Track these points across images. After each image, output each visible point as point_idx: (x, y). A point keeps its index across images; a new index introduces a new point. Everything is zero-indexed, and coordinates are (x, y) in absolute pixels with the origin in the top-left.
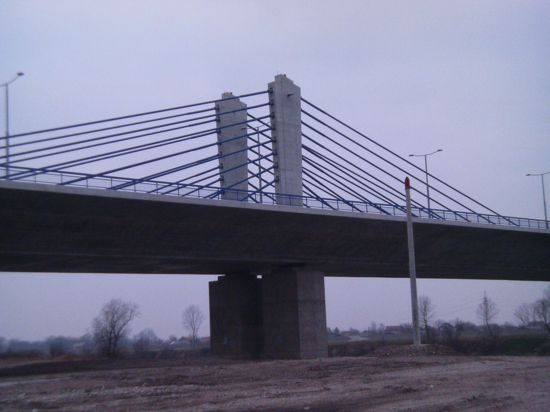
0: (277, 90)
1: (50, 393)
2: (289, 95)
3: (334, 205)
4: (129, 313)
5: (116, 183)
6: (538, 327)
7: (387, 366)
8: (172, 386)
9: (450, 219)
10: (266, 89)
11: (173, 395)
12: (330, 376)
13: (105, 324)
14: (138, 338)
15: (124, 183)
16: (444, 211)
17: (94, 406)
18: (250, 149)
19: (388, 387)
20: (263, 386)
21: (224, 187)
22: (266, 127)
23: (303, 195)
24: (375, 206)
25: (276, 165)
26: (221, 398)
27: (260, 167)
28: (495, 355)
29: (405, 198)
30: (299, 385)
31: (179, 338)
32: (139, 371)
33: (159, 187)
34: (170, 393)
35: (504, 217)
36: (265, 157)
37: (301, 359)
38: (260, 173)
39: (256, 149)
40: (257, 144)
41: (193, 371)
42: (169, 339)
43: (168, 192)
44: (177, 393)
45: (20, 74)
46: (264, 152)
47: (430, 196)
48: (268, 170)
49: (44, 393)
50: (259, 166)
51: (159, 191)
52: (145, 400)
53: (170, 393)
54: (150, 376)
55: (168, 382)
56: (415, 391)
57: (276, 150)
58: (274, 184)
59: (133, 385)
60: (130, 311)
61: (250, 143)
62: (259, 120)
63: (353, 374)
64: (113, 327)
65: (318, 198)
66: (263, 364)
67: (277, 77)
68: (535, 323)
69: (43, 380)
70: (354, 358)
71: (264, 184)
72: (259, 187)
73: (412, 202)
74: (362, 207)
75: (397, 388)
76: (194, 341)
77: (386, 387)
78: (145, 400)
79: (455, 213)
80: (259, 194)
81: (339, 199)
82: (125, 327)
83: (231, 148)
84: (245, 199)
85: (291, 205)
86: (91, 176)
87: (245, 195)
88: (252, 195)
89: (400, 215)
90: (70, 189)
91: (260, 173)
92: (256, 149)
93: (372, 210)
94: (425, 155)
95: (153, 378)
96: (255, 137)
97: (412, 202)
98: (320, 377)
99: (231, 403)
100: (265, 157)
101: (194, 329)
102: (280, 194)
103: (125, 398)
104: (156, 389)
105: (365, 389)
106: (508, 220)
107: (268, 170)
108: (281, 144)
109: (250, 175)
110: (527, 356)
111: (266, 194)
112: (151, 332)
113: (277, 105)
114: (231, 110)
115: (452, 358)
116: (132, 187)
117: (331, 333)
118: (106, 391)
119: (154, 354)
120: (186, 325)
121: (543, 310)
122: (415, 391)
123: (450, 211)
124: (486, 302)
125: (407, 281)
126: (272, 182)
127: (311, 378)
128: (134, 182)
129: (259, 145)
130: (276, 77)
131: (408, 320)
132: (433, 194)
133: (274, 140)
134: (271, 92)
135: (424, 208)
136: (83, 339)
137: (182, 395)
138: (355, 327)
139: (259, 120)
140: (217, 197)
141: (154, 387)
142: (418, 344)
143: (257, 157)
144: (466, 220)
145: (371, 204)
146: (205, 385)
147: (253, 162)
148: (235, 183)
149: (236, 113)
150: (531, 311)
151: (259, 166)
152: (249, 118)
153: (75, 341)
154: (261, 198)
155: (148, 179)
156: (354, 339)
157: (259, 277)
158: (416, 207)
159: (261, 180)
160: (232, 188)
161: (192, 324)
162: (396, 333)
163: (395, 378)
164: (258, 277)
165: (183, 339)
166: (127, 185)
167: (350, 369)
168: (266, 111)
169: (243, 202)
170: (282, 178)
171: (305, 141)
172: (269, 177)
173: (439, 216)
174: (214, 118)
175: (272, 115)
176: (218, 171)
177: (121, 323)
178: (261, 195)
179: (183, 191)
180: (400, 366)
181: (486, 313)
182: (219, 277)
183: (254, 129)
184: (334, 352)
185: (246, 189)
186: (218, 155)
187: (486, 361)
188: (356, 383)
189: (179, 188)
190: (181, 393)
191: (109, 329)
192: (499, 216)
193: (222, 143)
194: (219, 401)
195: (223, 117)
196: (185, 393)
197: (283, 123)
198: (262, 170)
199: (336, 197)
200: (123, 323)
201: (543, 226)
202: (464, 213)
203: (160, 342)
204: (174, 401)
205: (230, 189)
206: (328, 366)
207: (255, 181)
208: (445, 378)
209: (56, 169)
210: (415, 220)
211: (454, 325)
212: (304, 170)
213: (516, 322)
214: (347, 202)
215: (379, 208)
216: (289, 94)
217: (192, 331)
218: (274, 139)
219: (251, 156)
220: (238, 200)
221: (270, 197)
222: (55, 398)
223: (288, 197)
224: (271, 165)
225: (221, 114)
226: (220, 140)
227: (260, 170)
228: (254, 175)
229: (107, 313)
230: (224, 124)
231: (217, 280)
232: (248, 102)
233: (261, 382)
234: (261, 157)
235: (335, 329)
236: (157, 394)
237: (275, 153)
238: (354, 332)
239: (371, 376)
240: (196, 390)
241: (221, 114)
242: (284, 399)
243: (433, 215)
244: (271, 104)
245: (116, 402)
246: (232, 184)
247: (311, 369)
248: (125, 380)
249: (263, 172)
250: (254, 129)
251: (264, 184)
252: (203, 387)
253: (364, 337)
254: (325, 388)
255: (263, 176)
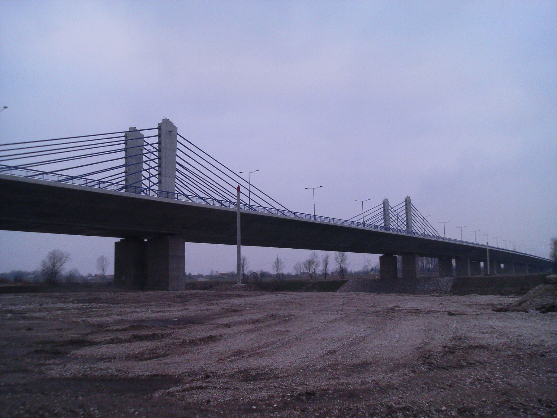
0: (163, 128)
1: (17, 305)
2: (170, 131)
3: (194, 200)
4: (63, 259)
5: (61, 178)
6: (306, 275)
7: (221, 296)
8: (93, 304)
9: (261, 211)
10: (157, 127)
11: (94, 309)
12: (188, 302)
13: (49, 264)
14: (68, 274)
15: (65, 178)
16: (258, 206)
17: (45, 314)
18: (144, 162)
19: (223, 309)
20: (148, 306)
21: (127, 184)
22: (155, 150)
23: (175, 192)
24: (218, 201)
25: (160, 173)
26: (123, 312)
27: (150, 174)
28: (282, 291)
29: (237, 198)
30: (170, 306)
31: (93, 275)
32: (72, 294)
33: (88, 182)
34: (91, 308)
35: (292, 212)
36: (154, 168)
37: (169, 290)
38: (150, 177)
39: (148, 163)
40: (149, 159)
41: (105, 295)
42: (87, 275)
43: (92, 186)
44: (96, 308)
45: (5, 107)
46: (153, 164)
47: (250, 197)
48: (154, 176)
49: (14, 305)
50: (149, 173)
51: (87, 184)
52: (77, 311)
53: (91, 308)
54: (78, 297)
55: (90, 301)
56: (238, 311)
57: (160, 164)
58: (158, 184)
59: (69, 302)
60: (65, 257)
61: (145, 159)
62: (151, 145)
63: (202, 301)
64: (54, 265)
65: (184, 194)
66: (147, 293)
67: (164, 120)
68: (304, 273)
69: (11, 297)
70: (202, 291)
71: (151, 184)
72: (148, 186)
73: (241, 201)
74: (210, 202)
75: (228, 309)
76: (103, 277)
77: (221, 308)
78: (77, 311)
79: (264, 208)
80: (148, 190)
81: (197, 196)
82: (62, 267)
83: (134, 161)
84: (140, 193)
85: (168, 198)
86: (45, 173)
87: (139, 190)
88: (144, 190)
89: (233, 208)
90: (29, 180)
91: (150, 177)
92: (148, 163)
93: (216, 203)
94: (249, 173)
95: (81, 298)
96: (148, 155)
97: (241, 201)
98: (182, 302)
99: (130, 315)
100: (154, 168)
101: (103, 270)
102: (161, 191)
103: (64, 310)
104: (83, 305)
105: (210, 309)
106: (294, 214)
107: (154, 176)
108: (163, 160)
109: (143, 178)
110: (299, 291)
111: (152, 190)
112: (76, 271)
113: (163, 137)
114: (134, 138)
115: (259, 293)
116: (71, 181)
117: (187, 276)
118: (52, 305)
119: (78, 284)
120: (99, 267)
121: (309, 266)
122: (238, 311)
123: (261, 206)
124: (278, 260)
125: (235, 247)
126: (157, 183)
127: (177, 302)
128: (72, 178)
129: (150, 160)
130: (163, 120)
131: (234, 270)
132: (252, 196)
133: (159, 158)
134: (159, 128)
135: (247, 204)
136: (34, 273)
137: (99, 310)
138: (201, 273)
139: (151, 145)
140: (123, 190)
141: (82, 304)
142: (240, 284)
143: (148, 167)
144: (271, 212)
145: (215, 200)
146: (114, 304)
147: (146, 170)
148: (134, 182)
149: (137, 140)
150: (302, 266)
151: (149, 173)
152: (145, 144)
153: (29, 274)
154: (149, 192)
155: (81, 177)
156: (200, 280)
157: (146, 240)
158: (242, 203)
159: (150, 181)
160: (133, 185)
161: (102, 267)
162: (225, 277)
163: (226, 303)
164: (147, 240)
165: (96, 276)
166: (68, 179)
167: (200, 297)
168: (156, 140)
169: (139, 194)
170: (163, 180)
171: (178, 160)
172: (155, 180)
173: (255, 209)
174: (124, 142)
175: (159, 142)
176: (124, 174)
177: (59, 264)
178: (149, 191)
179: (102, 185)
180: (229, 297)
181: (278, 266)
182: (121, 239)
183: (148, 150)
184: (188, 287)
185: (141, 187)
186: (124, 165)
187: (278, 295)
188: (204, 306)
189: (99, 184)
190: (99, 308)
191: (51, 268)
192: (289, 211)
193: (128, 158)
194: (122, 313)
195: (128, 142)
196: (101, 308)
197: (166, 148)
198: (151, 175)
199: (195, 195)
200: (60, 264)
201: (313, 218)
202: (270, 208)
203: (82, 277)
204: (95, 313)
205: (131, 186)
206: (187, 295)
207: (146, 182)
208: (255, 304)
209: (24, 167)
210: (241, 211)
211: (259, 273)
212: (177, 177)
213: (294, 273)
214: (202, 198)
215: (221, 203)
216: (170, 130)
217: (102, 271)
218: (159, 157)
219: (145, 166)
220: (136, 193)
221: (155, 192)
222: (21, 308)
223: (166, 193)
224: (157, 173)
225: (128, 140)
226: (126, 156)
227: (150, 175)
228: (146, 178)
229: (50, 258)
230: (129, 146)
231: (120, 241)
232: (145, 133)
233: (147, 304)
234: (151, 168)
235: (189, 273)
236: (84, 308)
237: (160, 166)
238: (200, 276)
239: (212, 302)
240: (107, 307)
241: (128, 140)
242: (161, 314)
243: (252, 209)
244: (159, 136)
245: (59, 312)
246: (132, 183)
247: (176, 297)
248: (63, 299)
249: (152, 177)
250: (148, 150)
251: (151, 184)
252: (111, 305)
253: (206, 279)
254: (186, 308)
255: (152, 179)
